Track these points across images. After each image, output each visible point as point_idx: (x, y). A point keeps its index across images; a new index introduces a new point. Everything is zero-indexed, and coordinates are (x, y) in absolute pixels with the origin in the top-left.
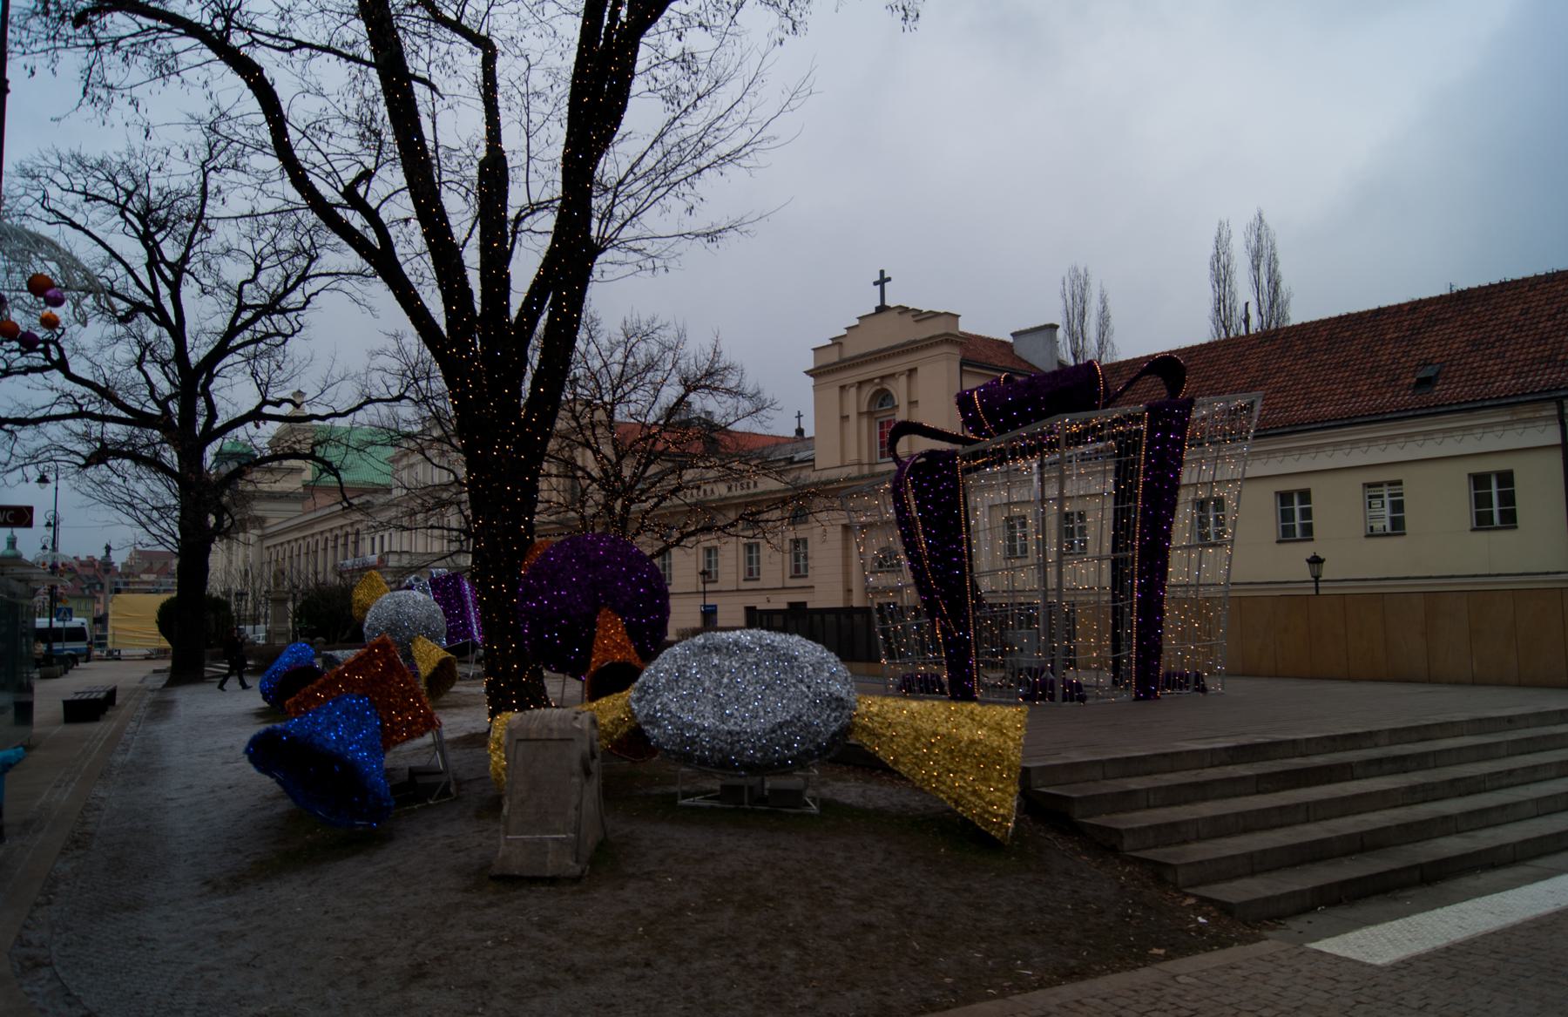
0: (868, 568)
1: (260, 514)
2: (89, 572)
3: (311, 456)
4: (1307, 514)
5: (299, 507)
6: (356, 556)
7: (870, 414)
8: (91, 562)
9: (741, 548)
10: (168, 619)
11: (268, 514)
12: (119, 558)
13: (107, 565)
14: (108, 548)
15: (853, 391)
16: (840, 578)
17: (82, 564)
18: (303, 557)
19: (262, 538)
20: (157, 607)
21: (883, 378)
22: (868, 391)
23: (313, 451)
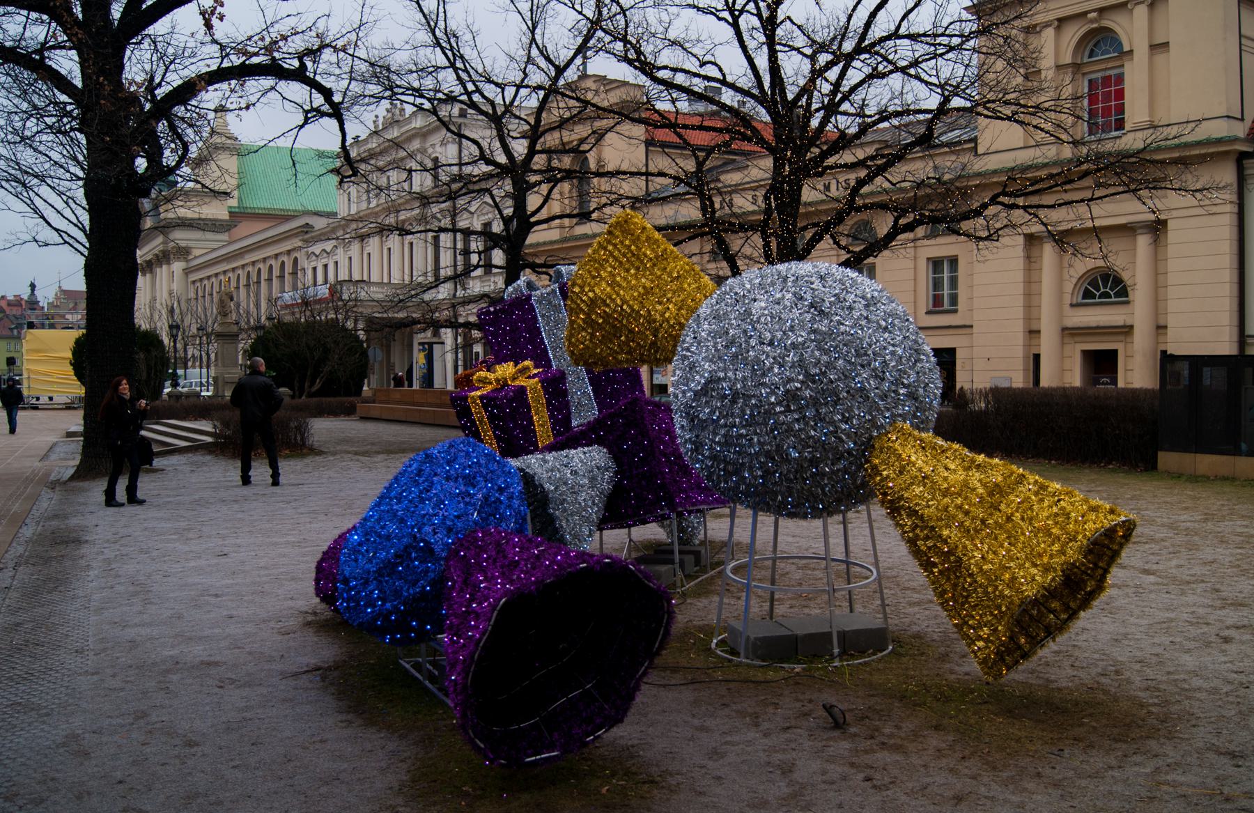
0: (1067, 299)
1: (183, 244)
2: (15, 311)
3: (299, 75)
4: (954, 282)
5: (224, 237)
6: (295, 288)
7: (1076, 67)
8: (17, 302)
9: (922, 264)
10: (85, 359)
11: (191, 244)
12: (46, 296)
13: (33, 304)
14: (33, 286)
15: (1049, 33)
16: (1019, 313)
17: (10, 304)
18: (242, 291)
19: (187, 272)
20: (71, 344)
21: (1101, 10)
22: (1073, 33)
23: (303, 66)
